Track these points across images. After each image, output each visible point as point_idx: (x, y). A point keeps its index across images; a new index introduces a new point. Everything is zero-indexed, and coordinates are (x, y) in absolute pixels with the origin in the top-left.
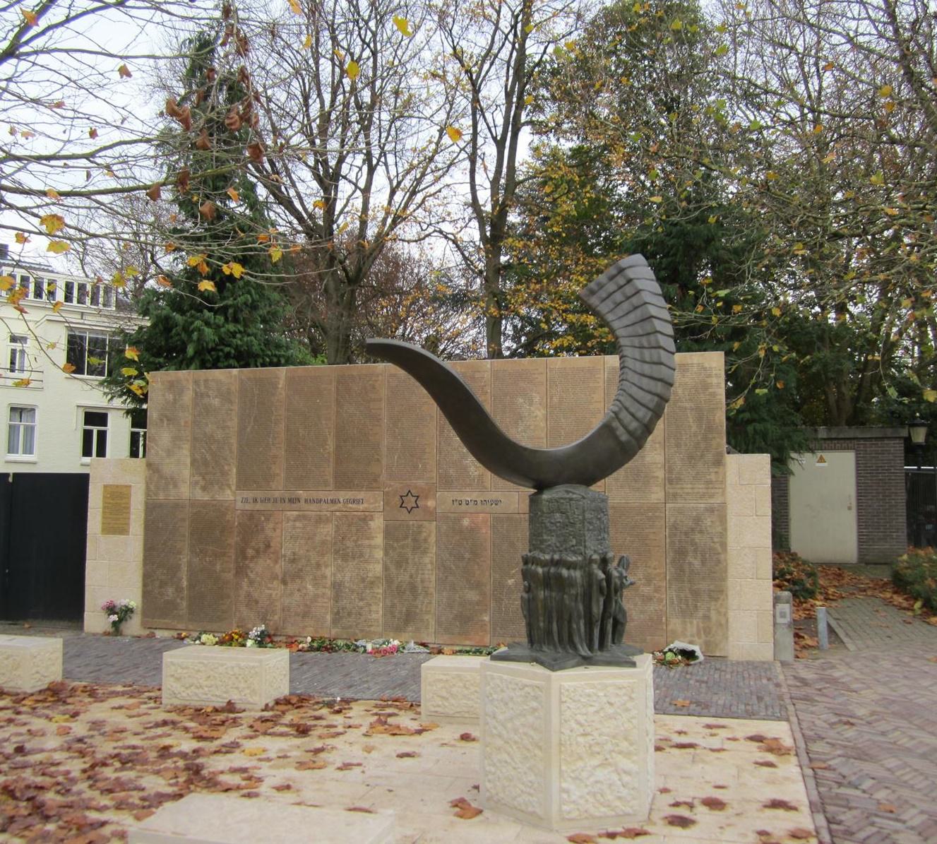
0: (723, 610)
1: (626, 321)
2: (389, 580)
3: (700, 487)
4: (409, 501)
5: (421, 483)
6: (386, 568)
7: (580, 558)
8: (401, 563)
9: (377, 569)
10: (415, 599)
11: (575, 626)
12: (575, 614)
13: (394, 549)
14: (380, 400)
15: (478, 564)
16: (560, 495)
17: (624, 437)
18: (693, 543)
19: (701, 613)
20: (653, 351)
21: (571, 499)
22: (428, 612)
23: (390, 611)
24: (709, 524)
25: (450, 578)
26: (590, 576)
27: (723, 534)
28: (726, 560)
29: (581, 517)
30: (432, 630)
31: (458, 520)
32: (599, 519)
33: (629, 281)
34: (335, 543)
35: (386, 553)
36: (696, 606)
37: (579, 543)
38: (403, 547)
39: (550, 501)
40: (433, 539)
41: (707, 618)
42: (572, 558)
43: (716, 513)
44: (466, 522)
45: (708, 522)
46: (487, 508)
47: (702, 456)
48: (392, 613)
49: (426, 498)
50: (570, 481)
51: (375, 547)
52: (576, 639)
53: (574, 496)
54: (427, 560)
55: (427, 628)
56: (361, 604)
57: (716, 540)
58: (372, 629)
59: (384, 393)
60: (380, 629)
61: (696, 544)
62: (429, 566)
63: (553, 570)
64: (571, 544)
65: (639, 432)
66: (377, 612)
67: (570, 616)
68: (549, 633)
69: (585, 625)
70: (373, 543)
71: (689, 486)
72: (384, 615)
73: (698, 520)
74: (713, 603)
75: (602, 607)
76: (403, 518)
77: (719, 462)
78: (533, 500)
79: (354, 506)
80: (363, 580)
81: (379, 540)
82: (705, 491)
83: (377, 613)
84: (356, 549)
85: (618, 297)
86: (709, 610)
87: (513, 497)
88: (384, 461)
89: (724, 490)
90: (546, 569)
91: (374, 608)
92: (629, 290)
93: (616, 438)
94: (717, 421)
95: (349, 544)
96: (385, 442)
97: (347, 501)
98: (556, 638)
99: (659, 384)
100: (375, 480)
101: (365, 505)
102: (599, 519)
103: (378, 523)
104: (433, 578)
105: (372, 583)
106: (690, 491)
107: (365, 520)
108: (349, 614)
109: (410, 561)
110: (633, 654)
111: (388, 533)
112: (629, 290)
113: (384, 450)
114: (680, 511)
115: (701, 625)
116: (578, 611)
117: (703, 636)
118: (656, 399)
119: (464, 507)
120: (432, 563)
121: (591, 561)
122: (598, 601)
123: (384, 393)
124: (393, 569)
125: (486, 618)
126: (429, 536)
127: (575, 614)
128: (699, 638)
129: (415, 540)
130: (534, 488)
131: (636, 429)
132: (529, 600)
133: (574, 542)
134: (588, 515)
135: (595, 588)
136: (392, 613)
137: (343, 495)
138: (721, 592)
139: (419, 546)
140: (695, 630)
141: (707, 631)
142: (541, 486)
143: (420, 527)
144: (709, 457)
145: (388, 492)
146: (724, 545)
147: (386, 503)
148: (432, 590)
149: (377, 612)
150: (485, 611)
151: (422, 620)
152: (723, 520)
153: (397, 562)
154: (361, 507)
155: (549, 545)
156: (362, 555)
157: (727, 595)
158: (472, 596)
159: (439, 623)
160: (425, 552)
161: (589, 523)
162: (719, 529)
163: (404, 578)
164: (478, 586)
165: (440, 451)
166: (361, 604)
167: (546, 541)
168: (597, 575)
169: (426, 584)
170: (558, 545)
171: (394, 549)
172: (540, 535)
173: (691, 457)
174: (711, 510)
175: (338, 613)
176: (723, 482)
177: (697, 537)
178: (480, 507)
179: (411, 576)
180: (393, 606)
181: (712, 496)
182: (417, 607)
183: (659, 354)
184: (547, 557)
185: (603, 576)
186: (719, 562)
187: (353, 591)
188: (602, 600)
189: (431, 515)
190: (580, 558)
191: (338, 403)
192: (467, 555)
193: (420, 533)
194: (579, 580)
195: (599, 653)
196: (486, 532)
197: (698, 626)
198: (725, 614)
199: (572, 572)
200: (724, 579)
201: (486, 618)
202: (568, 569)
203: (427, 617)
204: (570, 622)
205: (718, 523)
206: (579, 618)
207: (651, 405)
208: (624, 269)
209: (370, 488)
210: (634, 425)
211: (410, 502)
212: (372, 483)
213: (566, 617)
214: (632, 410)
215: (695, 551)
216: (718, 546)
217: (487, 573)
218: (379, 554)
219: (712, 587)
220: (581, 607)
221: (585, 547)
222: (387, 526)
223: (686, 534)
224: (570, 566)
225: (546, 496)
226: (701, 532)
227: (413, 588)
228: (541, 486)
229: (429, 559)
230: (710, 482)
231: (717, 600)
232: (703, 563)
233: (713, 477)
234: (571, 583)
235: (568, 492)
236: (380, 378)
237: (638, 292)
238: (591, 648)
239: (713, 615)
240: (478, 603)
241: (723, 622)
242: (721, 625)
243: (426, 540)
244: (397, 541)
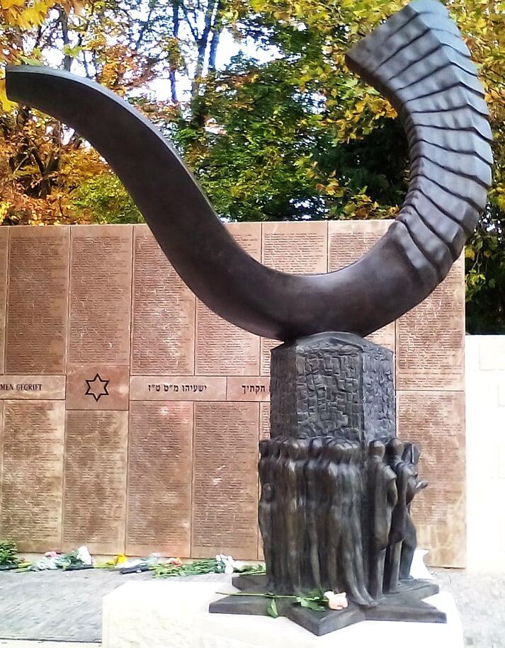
0: (461, 514)
1: (420, 89)
2: (71, 482)
3: (436, 372)
4: (96, 386)
5: (111, 366)
6: (67, 466)
7: (355, 447)
8: (85, 460)
9: (56, 468)
10: (101, 503)
11: (348, 556)
12: (350, 536)
13: (78, 444)
14: (63, 268)
15: (177, 459)
16: (323, 346)
17: (418, 261)
18: (428, 437)
19: (436, 517)
20: (462, 134)
21: (342, 353)
22: (117, 519)
23: (71, 517)
24: (445, 414)
25: (145, 477)
26: (371, 476)
27: (461, 426)
28: (464, 457)
29: (357, 381)
30: (121, 539)
31: (154, 410)
32: (381, 385)
33: (426, 31)
34: (6, 437)
35: (68, 449)
36: (430, 510)
37: (353, 422)
38: (88, 441)
39: (310, 355)
40: (124, 432)
41: (442, 523)
42: (347, 447)
43: (453, 402)
44: (164, 412)
45: (443, 412)
46: (191, 394)
47: (439, 335)
48: (73, 521)
49: (118, 383)
50: (334, 326)
51: (56, 441)
52: (351, 578)
53: (347, 347)
54: (117, 457)
55: (115, 537)
56: (36, 510)
57: (453, 433)
58: (49, 539)
59: (68, 260)
60: (58, 539)
61: (430, 437)
62: (119, 464)
63: (312, 465)
64: (340, 423)
65: (441, 255)
66: (55, 519)
67: (341, 540)
68: (306, 568)
69: (363, 554)
70: (51, 436)
71: (423, 371)
72: (64, 523)
73: (432, 410)
74: (450, 506)
75: (389, 525)
76: (90, 406)
77: (457, 344)
78: (278, 357)
79: (30, 393)
80: (39, 481)
81: (60, 432)
82: (441, 376)
83: (55, 520)
84: (31, 445)
85: (409, 54)
86: (445, 514)
87: (250, 351)
88: (67, 341)
89: (462, 376)
90: (301, 463)
91: (51, 514)
92: (424, 44)
93: (407, 262)
94: (456, 297)
95: (21, 437)
96: (68, 318)
97: (20, 387)
98: (317, 577)
99: (472, 183)
100: (56, 363)
101: (44, 392)
102: (381, 385)
103: (58, 414)
104: (124, 478)
105: (50, 484)
106: (424, 376)
107: (42, 409)
108: (21, 522)
109: (97, 457)
110: (426, 596)
111: (71, 424)
112: (424, 44)
113: (67, 326)
114: (412, 399)
115: (436, 531)
116: (353, 528)
117: (438, 544)
118: (466, 205)
119: (162, 393)
120: (122, 460)
121: (373, 450)
122: (385, 515)
123: (68, 260)
124: (76, 468)
125: (187, 525)
126: (120, 427)
127: (350, 536)
128: (434, 547)
129: (103, 433)
130: (279, 337)
131: (436, 251)
132: (272, 514)
133: (346, 421)
134: (366, 379)
135: (380, 494)
136: (73, 521)
137: (16, 380)
138: (459, 493)
139: (106, 439)
140: (429, 537)
141: (443, 538)
142: (290, 332)
143: (108, 417)
144: (446, 337)
145: (71, 376)
146: (462, 439)
147: (69, 389)
148: (122, 492)
149: (55, 519)
150: (185, 516)
151: (110, 529)
152: (461, 409)
153: (81, 459)
154: (38, 394)
155: (307, 426)
156: (38, 451)
157: (465, 497)
158: (170, 498)
159: (130, 531)
160: (115, 447)
161: (369, 390)
162: (457, 420)
163: (88, 477)
164: (177, 487)
165: (134, 327)
166: (36, 510)
167: (301, 418)
168: (383, 473)
169: (116, 485)
170: (320, 424)
171: (78, 444)
172: (293, 407)
173: (425, 338)
174: (449, 399)
175: (7, 521)
176: (462, 366)
177: (432, 429)
178: (181, 393)
179: (97, 476)
180: (75, 511)
181: (449, 383)
182: (103, 512)
183: (470, 138)
184: (303, 444)
185: (393, 475)
186: (456, 458)
187: (26, 495)
188: (390, 512)
189: (125, 404)
190: (355, 447)
191: (13, 270)
192: (165, 450)
193: (109, 424)
194: (354, 481)
195: (384, 598)
196: (188, 422)
197: (432, 532)
198: (463, 520)
199: (343, 467)
200: (461, 478)
201: (187, 525)
202: (338, 463)
203: (115, 524)
204: (340, 549)
205: (455, 414)
206: (354, 541)
207: (460, 217)
208: (417, 15)
209: (50, 372)
210: (433, 243)
211: (98, 388)
212: (51, 365)
213: (334, 541)
214: (432, 222)
215: (430, 445)
216: (455, 440)
217: (189, 472)
218: (59, 450)
219: (448, 488)
220: (357, 525)
221: (363, 427)
222: (69, 416)
223: (419, 425)
224: (339, 458)
225: (301, 347)
226: (436, 424)
227: (99, 490)
228: (290, 332)
229: (119, 456)
230: (446, 367)
231: (454, 502)
232: (439, 458)
233: (450, 361)
234: (344, 486)
235: (335, 342)
236: (64, 241)
237: (438, 47)
238: (372, 592)
239: (450, 518)
240: (177, 507)
241: (461, 527)
242: (458, 531)
243: (116, 433)
244: (81, 434)
